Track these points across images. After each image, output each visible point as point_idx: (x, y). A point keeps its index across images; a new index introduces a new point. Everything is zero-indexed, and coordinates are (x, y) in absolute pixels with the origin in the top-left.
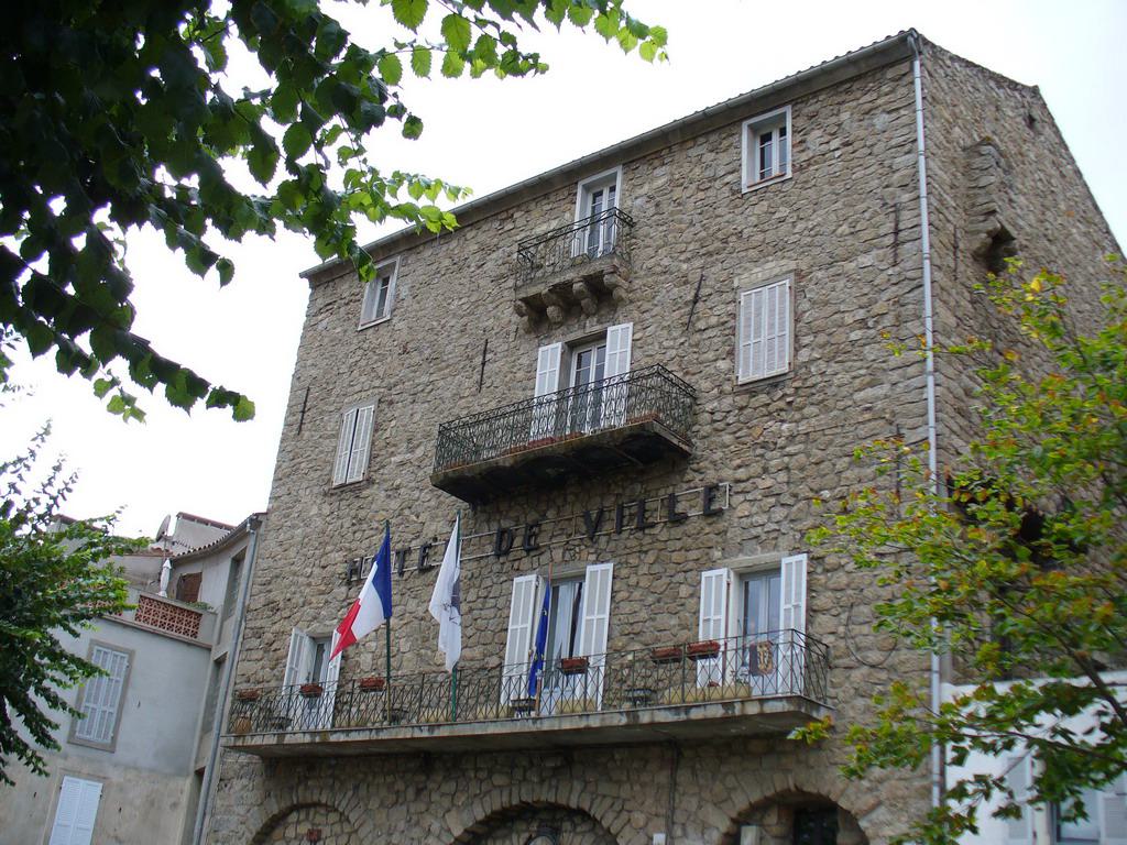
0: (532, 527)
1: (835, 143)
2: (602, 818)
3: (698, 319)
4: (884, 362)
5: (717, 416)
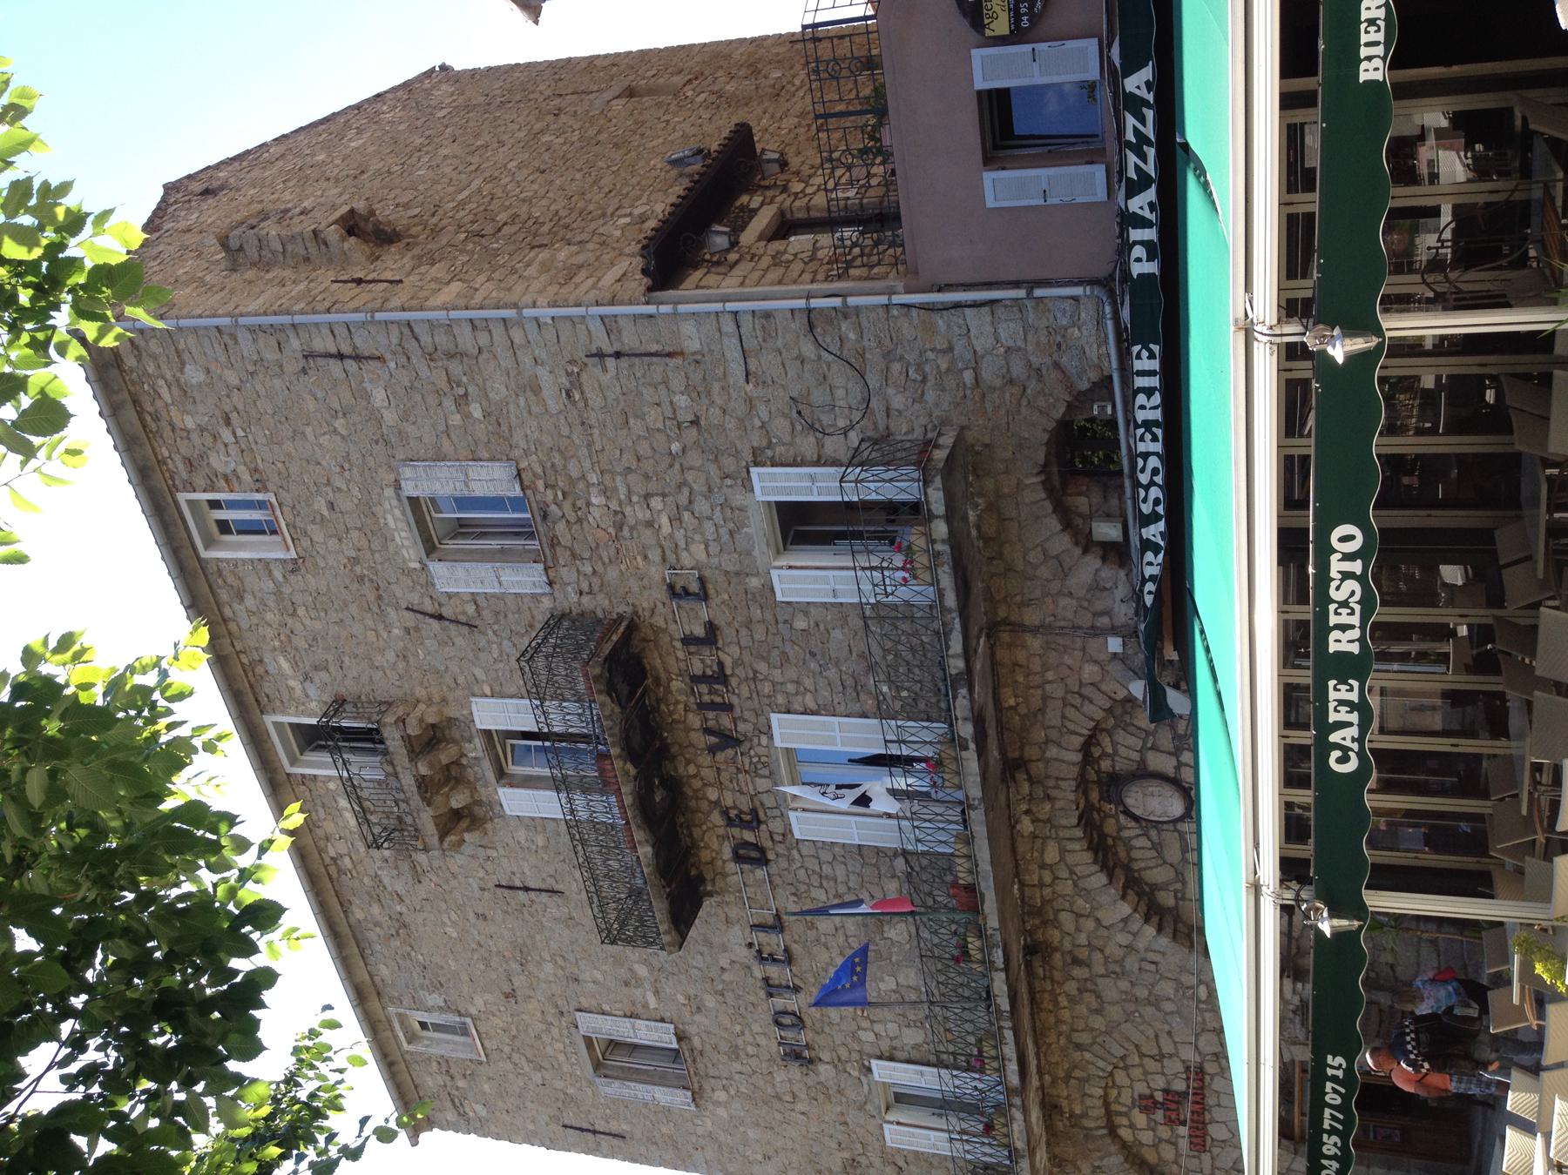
0: (729, 818)
1: (226, 435)
2: (1092, 719)
3: (464, 613)
4: (508, 374)
5: (585, 586)
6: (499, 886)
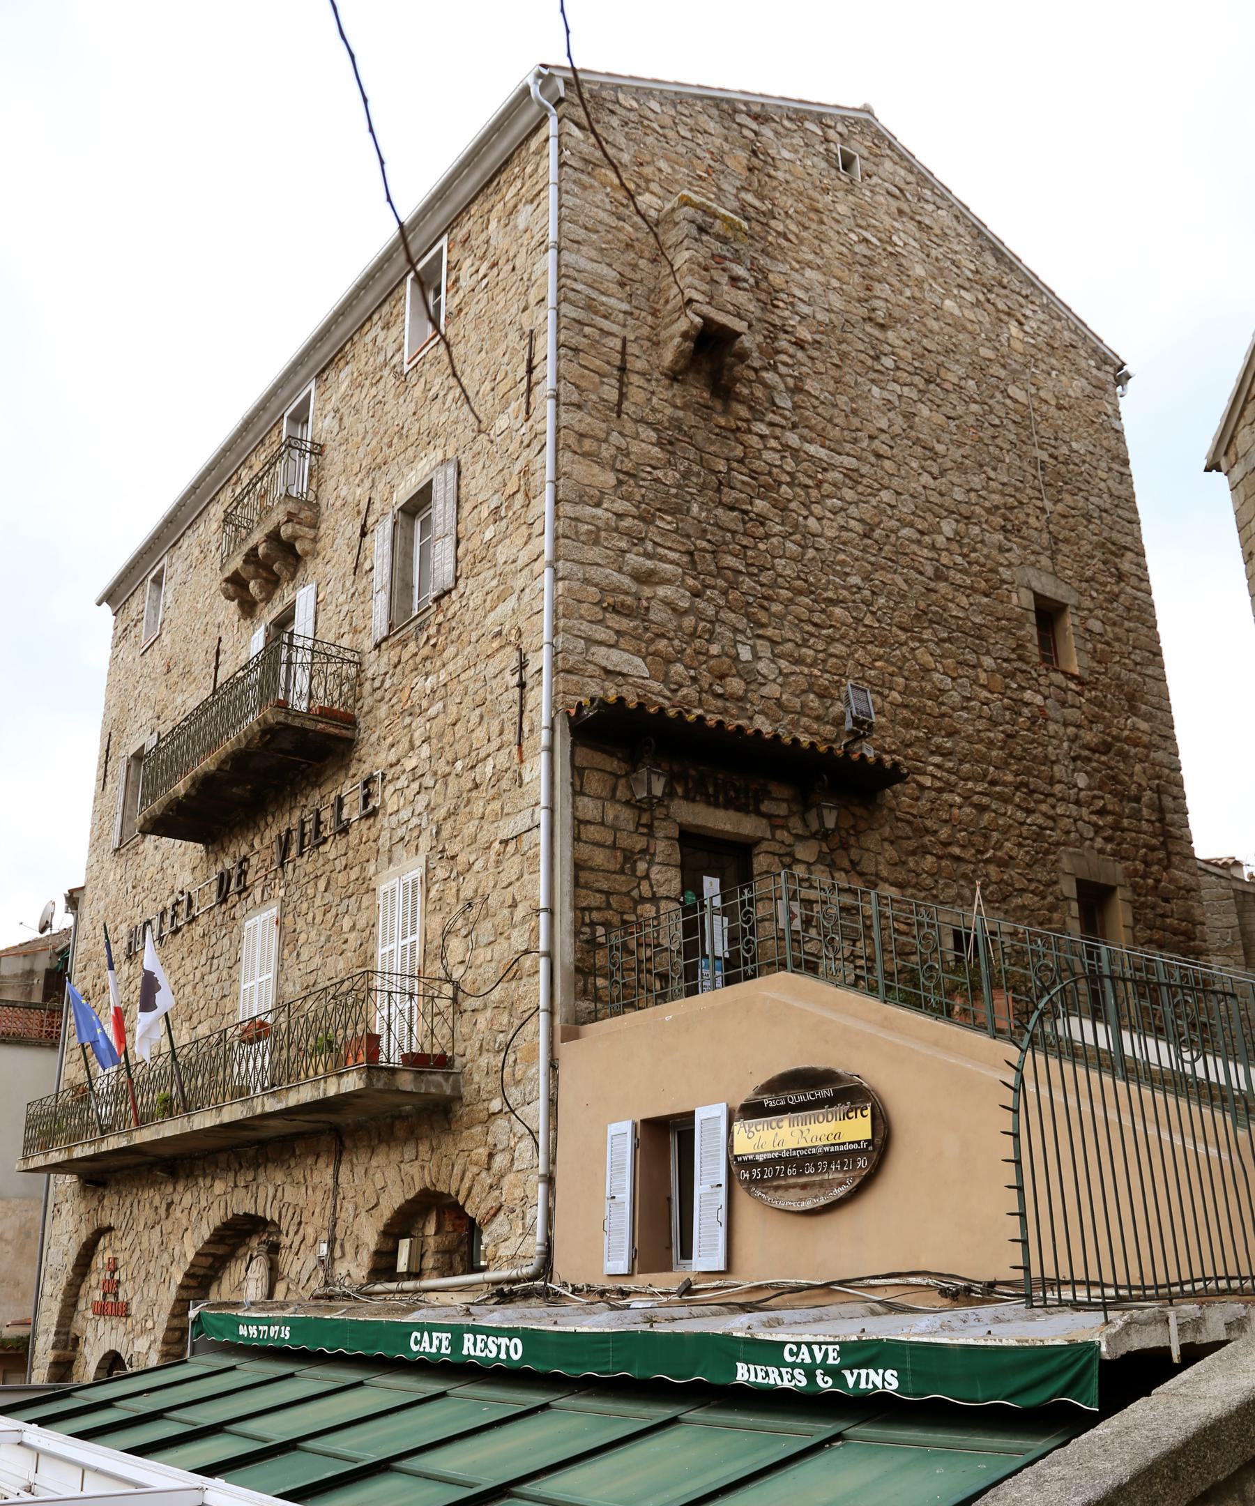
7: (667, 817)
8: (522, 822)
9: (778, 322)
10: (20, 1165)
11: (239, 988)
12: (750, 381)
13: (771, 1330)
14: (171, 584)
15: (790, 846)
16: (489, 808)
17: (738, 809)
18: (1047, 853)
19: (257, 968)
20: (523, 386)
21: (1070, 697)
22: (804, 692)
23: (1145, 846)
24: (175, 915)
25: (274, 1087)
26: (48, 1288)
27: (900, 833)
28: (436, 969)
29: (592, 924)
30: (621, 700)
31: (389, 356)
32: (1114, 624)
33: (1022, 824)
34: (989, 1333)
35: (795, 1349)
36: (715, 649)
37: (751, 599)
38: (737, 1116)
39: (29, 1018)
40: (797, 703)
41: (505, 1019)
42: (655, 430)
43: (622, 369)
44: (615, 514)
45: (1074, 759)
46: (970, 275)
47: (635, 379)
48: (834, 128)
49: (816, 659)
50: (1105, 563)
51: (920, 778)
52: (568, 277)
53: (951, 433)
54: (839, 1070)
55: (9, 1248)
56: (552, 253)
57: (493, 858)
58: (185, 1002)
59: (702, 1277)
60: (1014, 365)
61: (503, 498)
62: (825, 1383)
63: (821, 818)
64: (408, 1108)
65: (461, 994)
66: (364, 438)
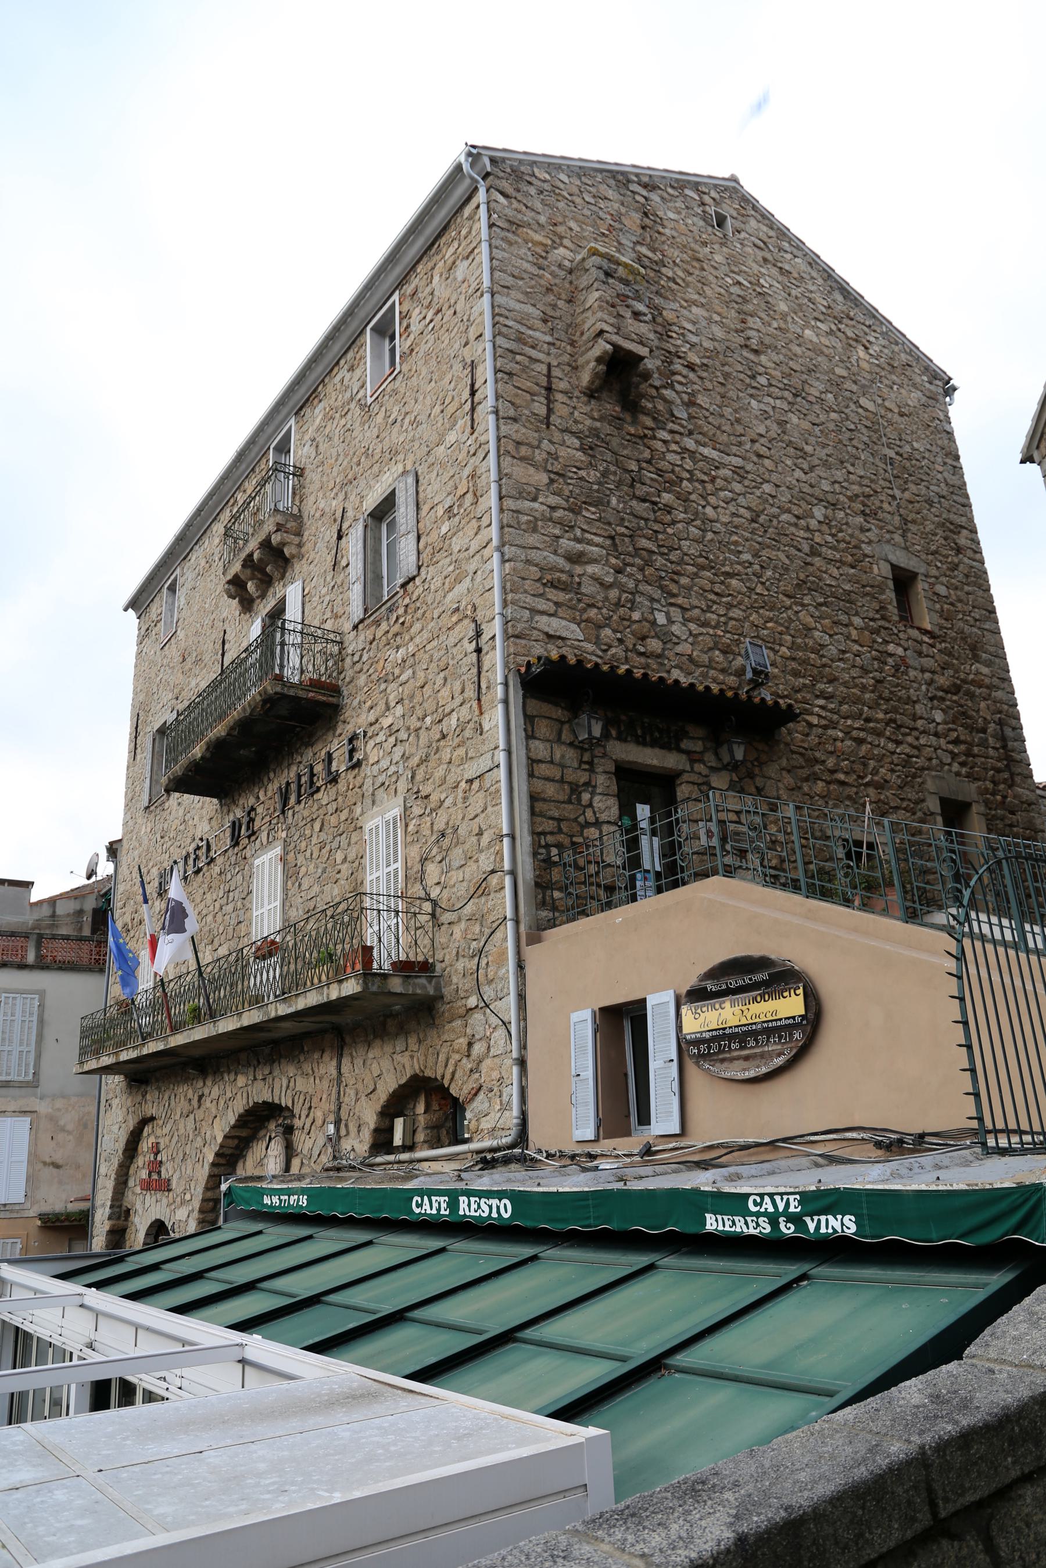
6: (225, 632)
7: (605, 755)
8: (484, 763)
9: (672, 349)
10: (76, 1069)
11: (252, 915)
12: (653, 397)
13: (733, 1183)
14: (184, 590)
15: (706, 776)
16: (455, 754)
17: (662, 747)
18: (914, 776)
19: (266, 899)
20: (468, 407)
21: (924, 648)
22: (710, 649)
23: (993, 769)
24: (197, 858)
25: (284, 995)
26: (103, 1170)
27: (796, 764)
28: (417, 890)
29: (547, 846)
30: (563, 658)
31: (355, 392)
32: (956, 588)
33: (893, 753)
34: (938, 1178)
35: (759, 1200)
36: (636, 616)
37: (663, 574)
38: (683, 1000)
39: (80, 949)
40: (705, 658)
41: (477, 929)
42: (578, 438)
43: (549, 389)
44: (549, 506)
45: (931, 699)
46: (824, 310)
47: (559, 397)
48: (708, 194)
49: (718, 622)
50: (945, 539)
51: (808, 718)
52: (501, 315)
53: (816, 437)
54: (773, 957)
55: (71, 1137)
56: (487, 297)
57: (461, 795)
58: (207, 928)
59: (660, 1140)
60: (863, 381)
61: (455, 499)
62: (787, 1229)
63: (731, 752)
64: (397, 1007)
65: (438, 910)
66: (336, 460)
